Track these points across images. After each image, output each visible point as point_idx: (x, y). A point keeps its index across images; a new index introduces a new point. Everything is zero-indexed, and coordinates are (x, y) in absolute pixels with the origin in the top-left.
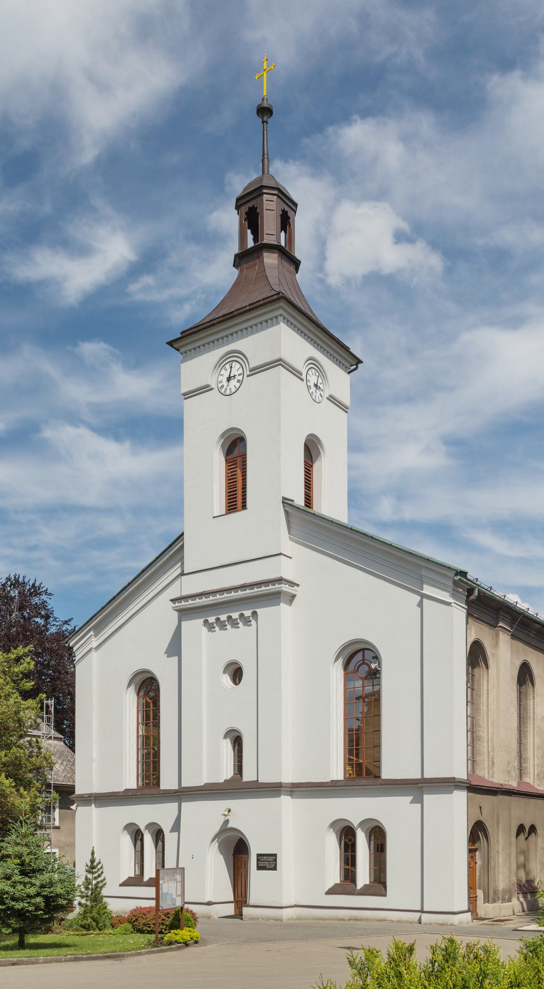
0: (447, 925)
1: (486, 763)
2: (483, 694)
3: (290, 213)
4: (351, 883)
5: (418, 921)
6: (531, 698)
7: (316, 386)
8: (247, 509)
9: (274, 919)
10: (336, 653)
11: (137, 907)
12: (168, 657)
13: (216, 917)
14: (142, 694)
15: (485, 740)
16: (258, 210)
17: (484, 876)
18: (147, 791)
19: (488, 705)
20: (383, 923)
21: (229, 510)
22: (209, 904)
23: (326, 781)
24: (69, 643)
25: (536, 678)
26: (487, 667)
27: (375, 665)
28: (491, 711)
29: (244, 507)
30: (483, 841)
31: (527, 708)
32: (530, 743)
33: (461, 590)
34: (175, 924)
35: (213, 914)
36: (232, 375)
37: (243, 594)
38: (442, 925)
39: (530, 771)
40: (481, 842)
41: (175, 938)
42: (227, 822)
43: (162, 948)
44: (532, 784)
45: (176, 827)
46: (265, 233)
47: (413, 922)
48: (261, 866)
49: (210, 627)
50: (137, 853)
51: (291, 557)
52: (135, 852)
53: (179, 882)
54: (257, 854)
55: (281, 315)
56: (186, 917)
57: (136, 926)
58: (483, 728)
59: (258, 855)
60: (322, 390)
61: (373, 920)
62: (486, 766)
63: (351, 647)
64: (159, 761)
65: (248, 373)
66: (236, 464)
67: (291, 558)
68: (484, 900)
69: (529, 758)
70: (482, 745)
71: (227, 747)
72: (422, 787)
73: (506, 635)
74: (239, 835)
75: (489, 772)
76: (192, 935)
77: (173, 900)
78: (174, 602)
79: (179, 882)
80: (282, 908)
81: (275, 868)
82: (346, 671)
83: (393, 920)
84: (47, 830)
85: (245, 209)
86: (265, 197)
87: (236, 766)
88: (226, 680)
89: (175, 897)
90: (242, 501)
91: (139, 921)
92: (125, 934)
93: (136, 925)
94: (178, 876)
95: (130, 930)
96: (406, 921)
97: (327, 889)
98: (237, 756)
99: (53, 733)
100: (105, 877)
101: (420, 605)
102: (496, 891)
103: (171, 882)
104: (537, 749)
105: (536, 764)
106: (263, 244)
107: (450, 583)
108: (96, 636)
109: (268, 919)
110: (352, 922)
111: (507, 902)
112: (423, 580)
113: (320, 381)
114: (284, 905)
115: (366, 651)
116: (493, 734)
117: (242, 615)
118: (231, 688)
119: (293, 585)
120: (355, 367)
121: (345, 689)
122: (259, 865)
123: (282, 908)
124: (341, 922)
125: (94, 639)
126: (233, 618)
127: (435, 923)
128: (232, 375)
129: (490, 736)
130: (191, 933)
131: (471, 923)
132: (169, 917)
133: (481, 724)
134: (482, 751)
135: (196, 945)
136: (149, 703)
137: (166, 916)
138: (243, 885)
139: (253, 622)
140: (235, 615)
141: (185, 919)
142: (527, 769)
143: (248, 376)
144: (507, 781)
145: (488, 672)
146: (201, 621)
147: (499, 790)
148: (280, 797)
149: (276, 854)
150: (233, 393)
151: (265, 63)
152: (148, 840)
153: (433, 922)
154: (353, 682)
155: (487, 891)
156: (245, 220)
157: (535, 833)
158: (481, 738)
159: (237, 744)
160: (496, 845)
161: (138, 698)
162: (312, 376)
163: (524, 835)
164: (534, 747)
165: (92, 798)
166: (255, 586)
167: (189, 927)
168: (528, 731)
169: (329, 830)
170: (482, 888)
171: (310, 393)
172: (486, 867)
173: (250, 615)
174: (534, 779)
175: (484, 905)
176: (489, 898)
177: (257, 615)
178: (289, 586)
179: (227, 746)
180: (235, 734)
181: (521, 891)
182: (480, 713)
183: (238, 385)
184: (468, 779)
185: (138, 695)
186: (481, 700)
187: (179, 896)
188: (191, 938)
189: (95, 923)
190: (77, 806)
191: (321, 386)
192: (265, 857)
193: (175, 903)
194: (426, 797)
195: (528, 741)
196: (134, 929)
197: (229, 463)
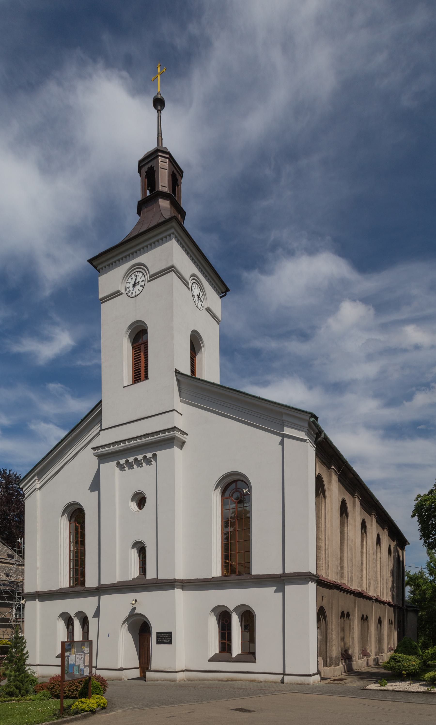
0: (305, 684)
1: (324, 566)
2: (322, 516)
3: (178, 177)
4: (227, 653)
5: (281, 681)
6: (346, 525)
7: (198, 297)
8: (148, 379)
9: (169, 681)
10: (216, 483)
11: (56, 676)
12: (91, 492)
13: (126, 679)
14: (73, 520)
15: (323, 549)
16: (155, 169)
17: (323, 647)
18: (77, 589)
19: (325, 524)
20: (253, 683)
21: (135, 381)
22: (121, 670)
23: (209, 577)
24: (20, 485)
25: (349, 512)
26: (325, 497)
27: (246, 490)
28: (327, 528)
29: (146, 378)
30: (323, 622)
31: (343, 532)
32: (345, 556)
33: (313, 432)
34: (85, 691)
35: (123, 677)
36: (137, 282)
37: (146, 440)
38: (300, 684)
39: (345, 576)
40: (321, 622)
41: (82, 707)
42: (134, 609)
43: (66, 719)
44: (346, 584)
45: (97, 614)
46: (160, 185)
47: (277, 682)
48: (160, 641)
49: (121, 467)
50: (69, 634)
51: (182, 414)
52: (68, 633)
53: (87, 653)
54: (157, 632)
55: (173, 234)
56: (95, 685)
57: (54, 692)
58: (322, 540)
59: (158, 633)
60: (203, 302)
61: (245, 681)
62: (324, 568)
63: (228, 478)
64: (85, 567)
65: (149, 279)
66: (140, 349)
67: (181, 415)
68: (323, 664)
69: (344, 566)
70: (321, 552)
71: (134, 554)
72: (284, 580)
73: (336, 476)
74: (144, 619)
75: (326, 572)
76: (100, 702)
77: (81, 671)
78: (94, 449)
79: (87, 653)
80: (176, 672)
81: (170, 643)
82: (223, 497)
83: (261, 681)
84: (19, 622)
85: (145, 169)
86: (160, 159)
87: (141, 569)
88: (134, 506)
89: (83, 668)
90: (144, 368)
91: (56, 688)
92: (43, 700)
93: (53, 691)
94: (86, 648)
95: (48, 696)
96: (271, 681)
97: (209, 658)
98: (141, 562)
99: (22, 560)
100: (28, 651)
101: (282, 443)
102: (331, 658)
103: (78, 654)
104: (350, 560)
105: (349, 571)
106: (159, 191)
107: (306, 425)
108: (39, 480)
109: (165, 680)
110: (229, 682)
111: (337, 666)
112: (284, 424)
113: (201, 295)
114: (177, 670)
115: (238, 482)
116: (328, 545)
117: (145, 457)
118: (138, 511)
119: (183, 434)
120: (224, 294)
121: (223, 510)
122: (158, 640)
123: (176, 672)
124: (220, 682)
125: (37, 482)
126: (138, 459)
127: (295, 683)
128: (137, 282)
129: (326, 546)
130: (99, 700)
131: (320, 682)
132: (81, 684)
133: (321, 537)
134: (321, 557)
135: (103, 711)
136: (78, 526)
137: (79, 683)
138: (146, 656)
139: (154, 462)
140: (140, 457)
141: (94, 687)
142: (344, 574)
143: (149, 281)
144: (337, 580)
145: (325, 500)
146: (115, 463)
147: (333, 585)
148: (174, 589)
149: (171, 632)
150: (138, 295)
151: (159, 69)
152: (77, 624)
153: (293, 682)
154: (228, 506)
155: (325, 658)
156: (145, 178)
157: (349, 618)
158: (320, 548)
159: (141, 553)
160: (331, 625)
161: (70, 524)
162: (195, 289)
163: (344, 619)
164: (348, 559)
165: (36, 595)
166: (155, 434)
167: (98, 694)
168: (344, 548)
169: (211, 613)
170: (322, 656)
171: (194, 300)
172: (324, 641)
173: (151, 456)
174: (348, 580)
175: (324, 668)
176: (326, 663)
177: (157, 456)
178: (180, 433)
179: (134, 555)
180: (141, 545)
181: (343, 658)
182: (320, 529)
183: (141, 289)
184: (317, 574)
185: (70, 521)
186: (320, 520)
187: (87, 666)
188: (99, 705)
189: (18, 690)
190: (26, 601)
191: (202, 298)
192: (162, 635)
193: (82, 674)
194: (287, 587)
195: (344, 554)
196: (52, 694)
197: (135, 349)
